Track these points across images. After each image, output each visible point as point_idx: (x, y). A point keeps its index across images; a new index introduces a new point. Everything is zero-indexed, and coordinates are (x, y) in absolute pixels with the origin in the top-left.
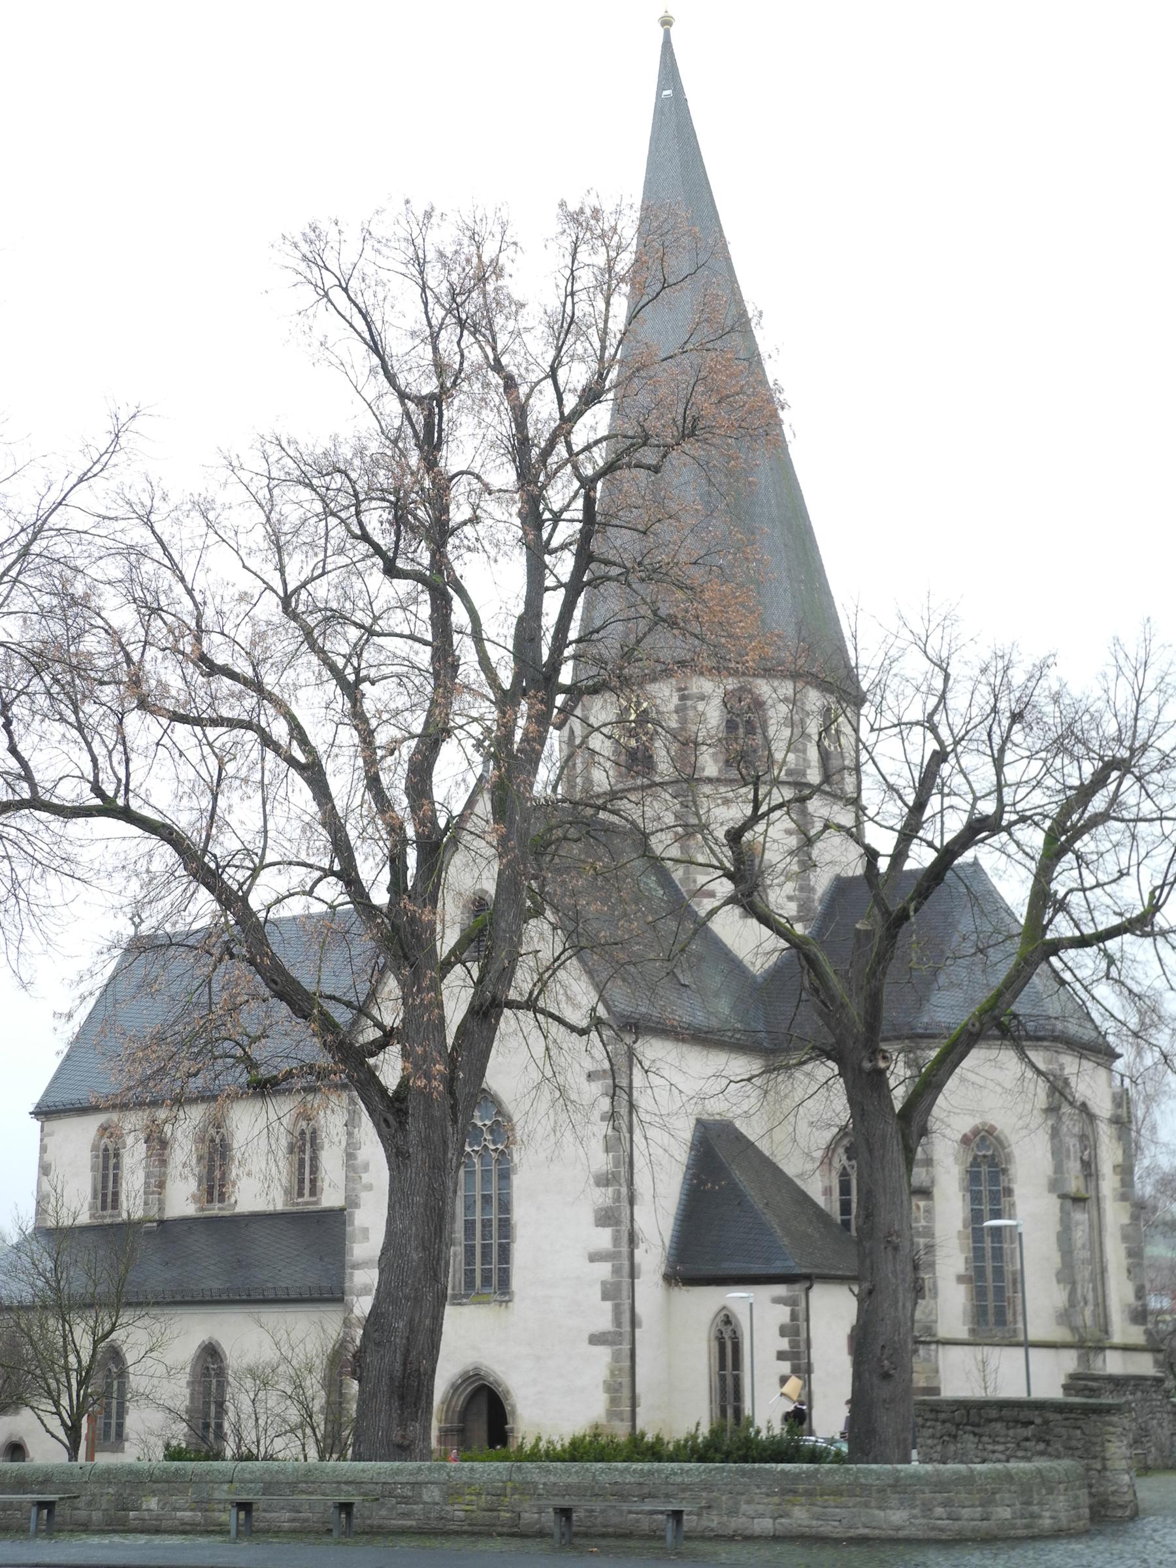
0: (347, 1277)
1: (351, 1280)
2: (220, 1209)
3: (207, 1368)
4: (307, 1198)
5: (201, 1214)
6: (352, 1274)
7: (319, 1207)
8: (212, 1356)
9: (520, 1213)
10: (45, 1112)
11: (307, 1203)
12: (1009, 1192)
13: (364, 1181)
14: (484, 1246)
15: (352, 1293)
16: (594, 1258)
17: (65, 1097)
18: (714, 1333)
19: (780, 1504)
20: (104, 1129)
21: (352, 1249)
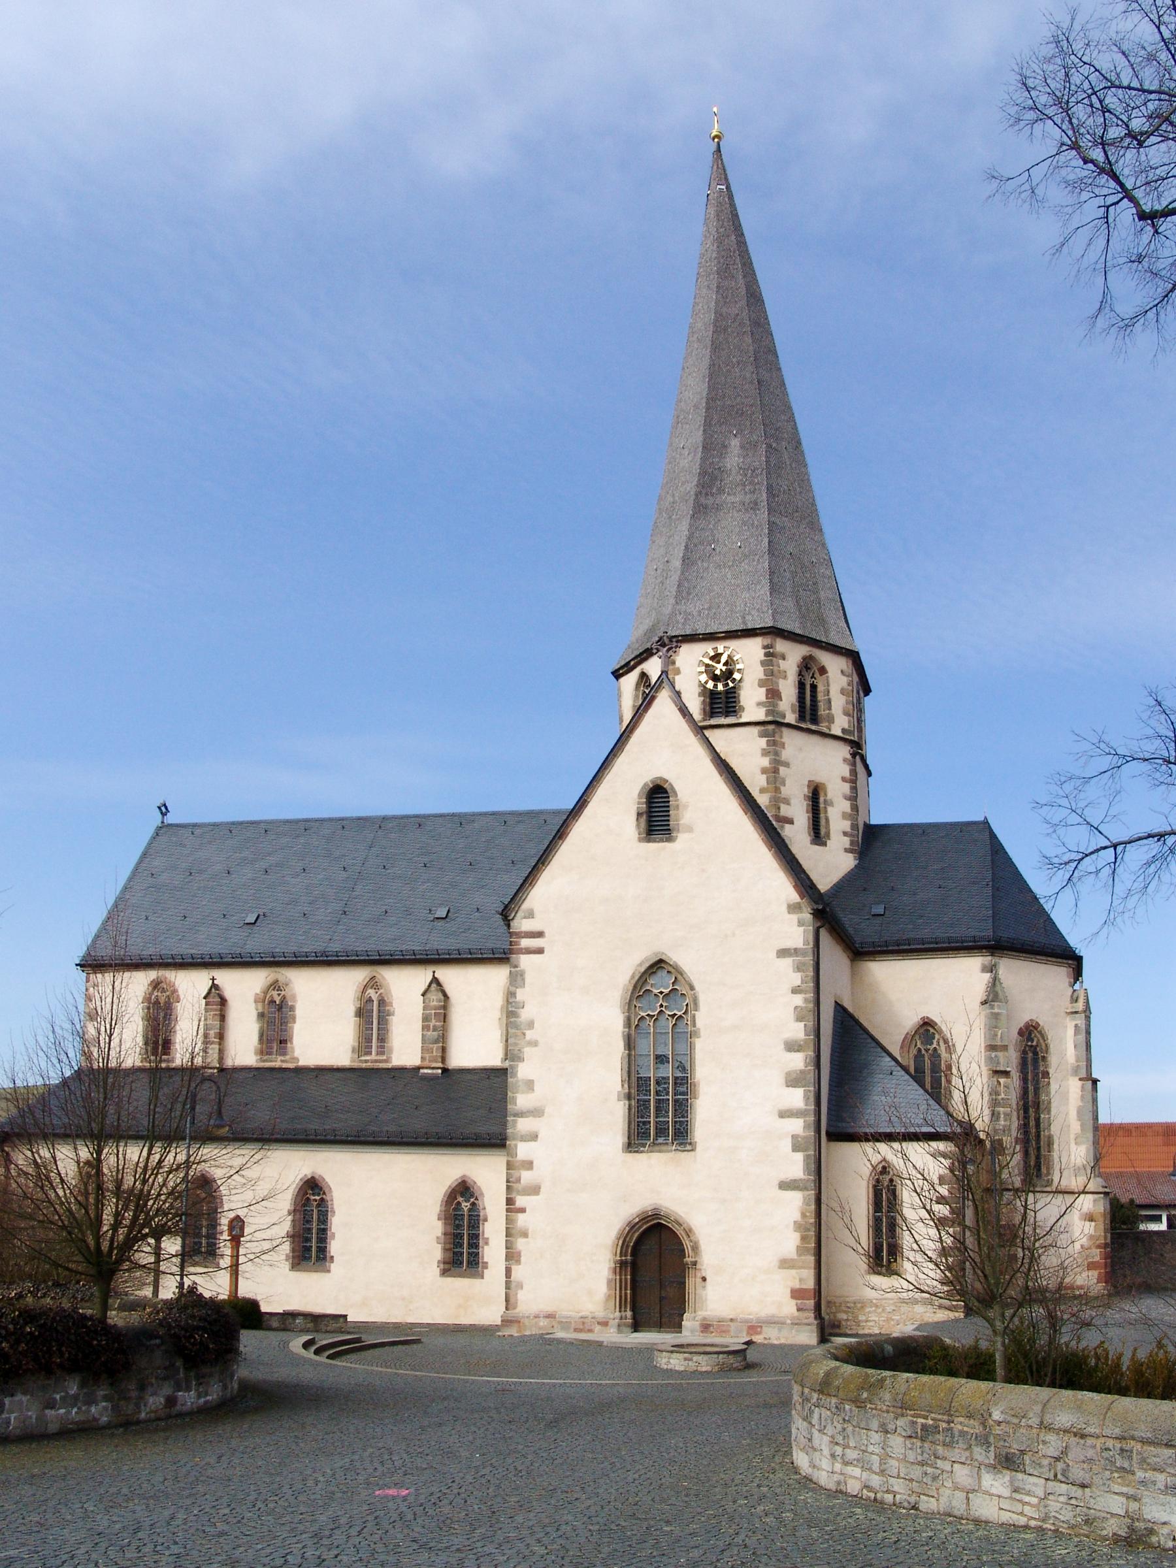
0: (509, 1125)
1: (514, 1126)
2: (282, 1061)
3: (308, 1199)
4: (373, 1057)
5: (262, 1065)
6: (515, 1122)
7: (390, 1065)
8: (312, 1189)
9: (704, 1072)
10: (92, 964)
11: (376, 1061)
12: (1046, 1074)
13: (528, 1037)
14: (658, 1102)
15: (514, 1139)
16: (784, 1114)
17: (105, 951)
18: (872, 1182)
19: (118, 1192)
20: (156, 985)
21: (514, 1099)
